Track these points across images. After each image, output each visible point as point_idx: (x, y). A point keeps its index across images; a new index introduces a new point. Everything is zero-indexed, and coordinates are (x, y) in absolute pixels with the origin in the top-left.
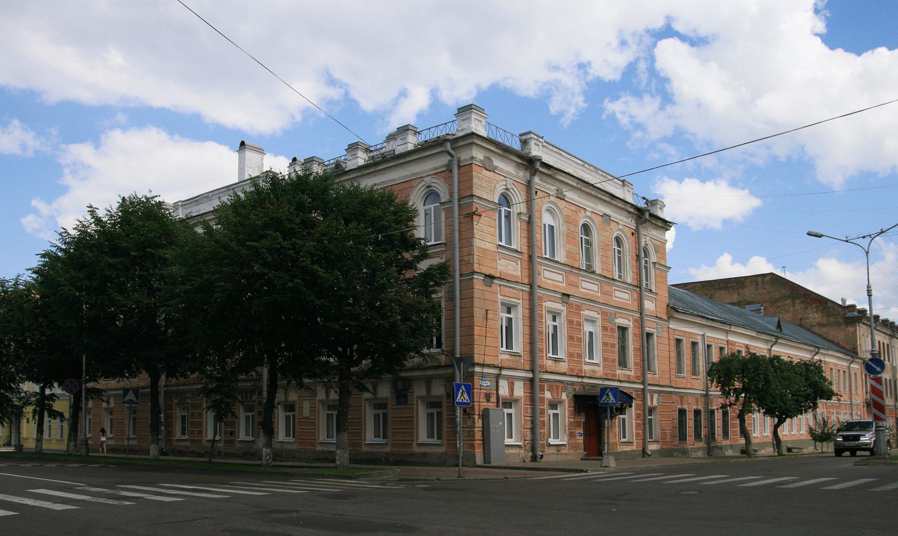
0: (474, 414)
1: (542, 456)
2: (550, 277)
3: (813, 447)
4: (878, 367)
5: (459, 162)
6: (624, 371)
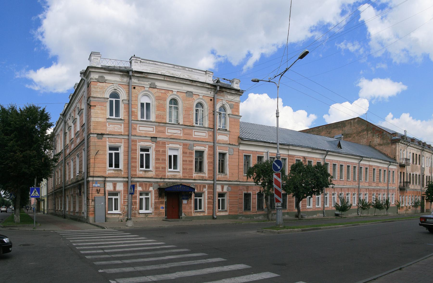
3: (356, 213)
6: (199, 175)
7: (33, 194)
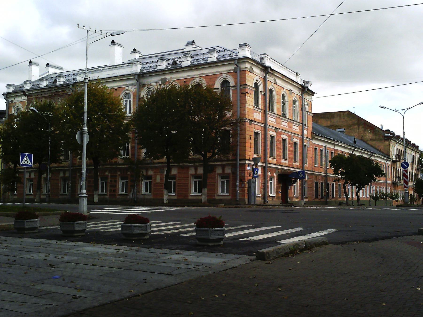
0: (245, 182)
1: (268, 201)
2: (271, 120)
4: (406, 165)
5: (240, 69)
7: (24, 161)
